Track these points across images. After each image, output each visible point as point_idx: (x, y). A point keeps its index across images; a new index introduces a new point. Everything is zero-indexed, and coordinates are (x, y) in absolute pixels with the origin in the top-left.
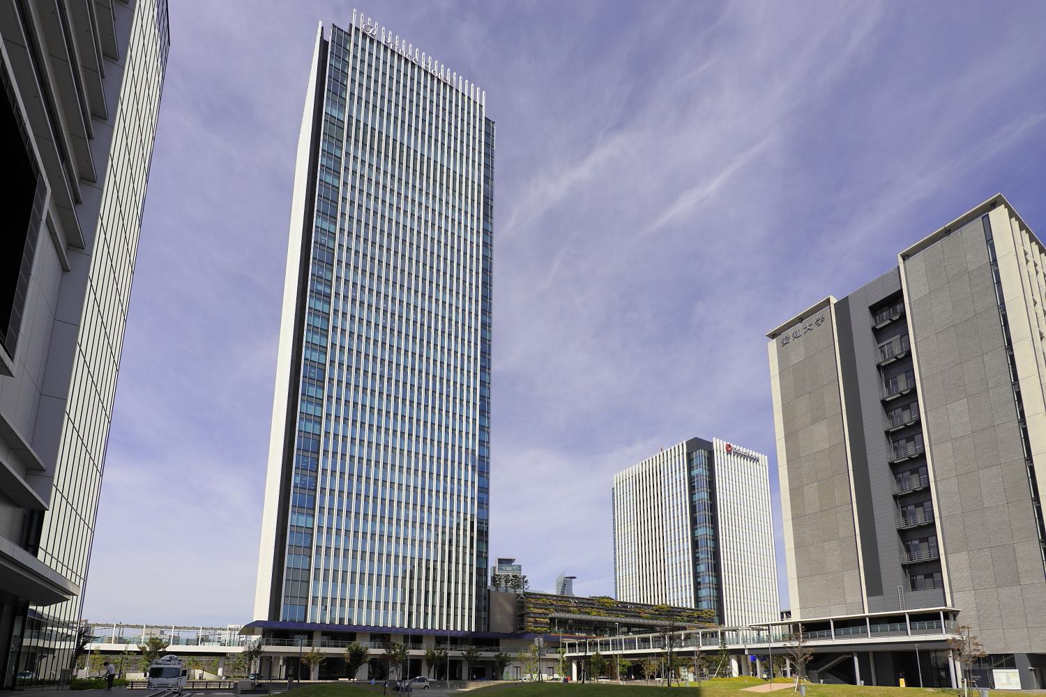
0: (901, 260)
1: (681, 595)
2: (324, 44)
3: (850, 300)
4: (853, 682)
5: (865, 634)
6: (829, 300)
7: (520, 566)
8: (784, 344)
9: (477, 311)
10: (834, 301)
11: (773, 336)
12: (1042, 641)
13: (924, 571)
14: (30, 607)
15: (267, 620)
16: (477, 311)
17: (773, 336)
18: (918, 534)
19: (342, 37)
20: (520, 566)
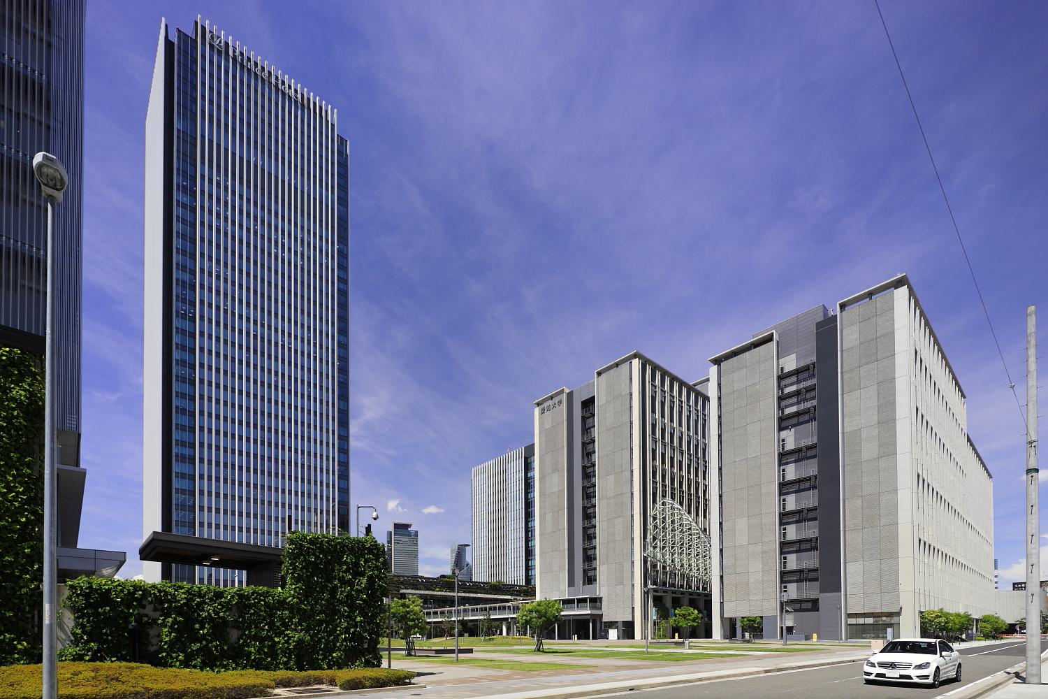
0: (596, 375)
1: (516, 576)
2: (169, 45)
3: (574, 393)
4: (589, 639)
5: (572, 609)
6: (563, 389)
7: (417, 532)
8: (543, 412)
9: (334, 521)
10: (567, 391)
11: (538, 404)
12: (1031, 650)
13: (590, 579)
14: (29, 550)
15: (160, 564)
16: (334, 521)
17: (538, 404)
18: (589, 558)
19: (188, 43)
20: (417, 532)
